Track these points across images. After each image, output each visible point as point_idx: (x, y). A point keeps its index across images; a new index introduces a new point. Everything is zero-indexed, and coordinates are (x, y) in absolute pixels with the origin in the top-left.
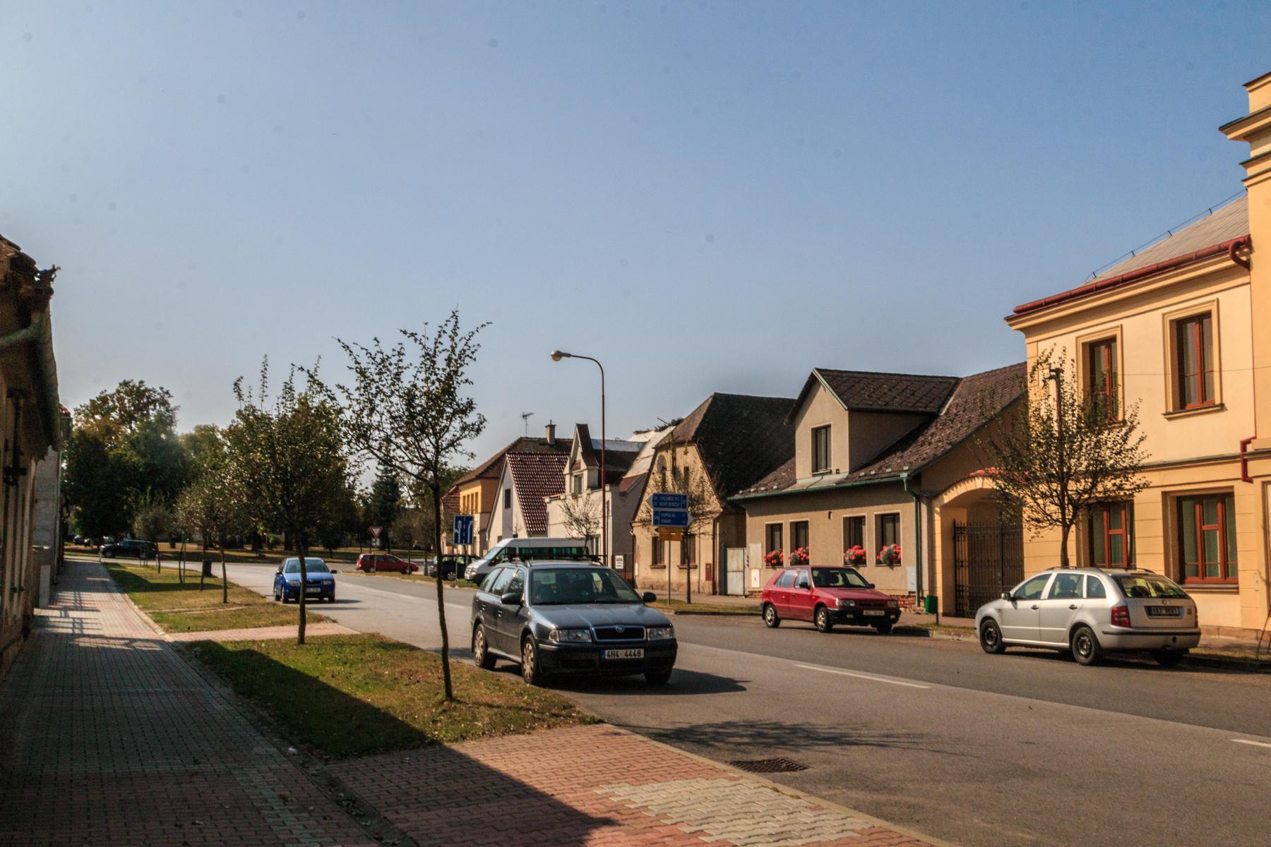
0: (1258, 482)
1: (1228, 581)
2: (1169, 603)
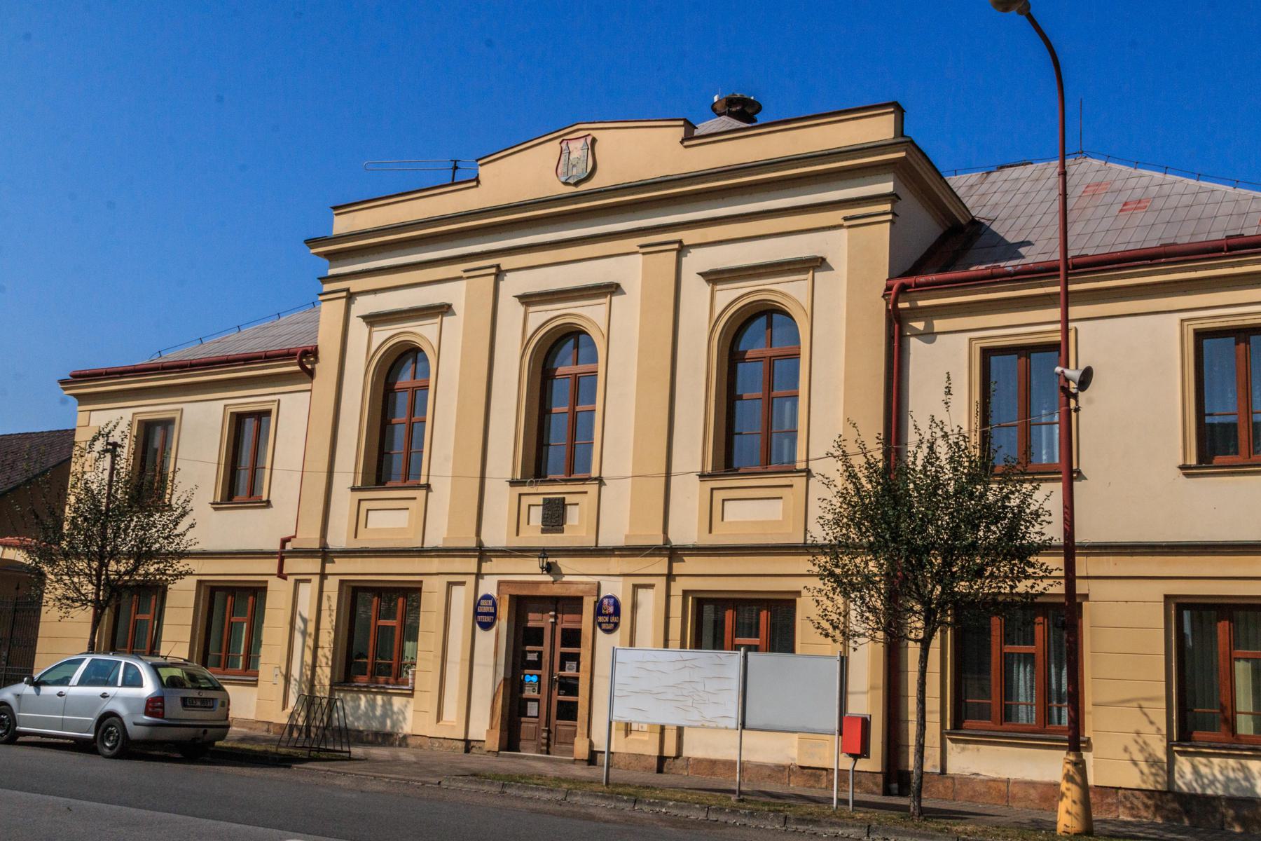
0: (291, 579)
1: (249, 674)
2: (205, 694)
